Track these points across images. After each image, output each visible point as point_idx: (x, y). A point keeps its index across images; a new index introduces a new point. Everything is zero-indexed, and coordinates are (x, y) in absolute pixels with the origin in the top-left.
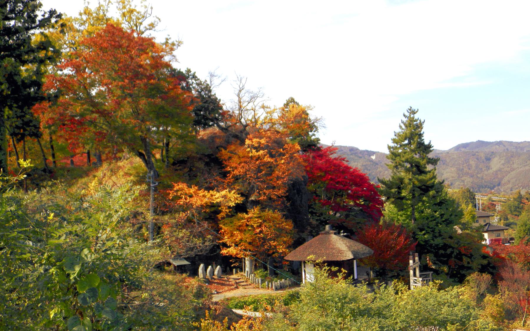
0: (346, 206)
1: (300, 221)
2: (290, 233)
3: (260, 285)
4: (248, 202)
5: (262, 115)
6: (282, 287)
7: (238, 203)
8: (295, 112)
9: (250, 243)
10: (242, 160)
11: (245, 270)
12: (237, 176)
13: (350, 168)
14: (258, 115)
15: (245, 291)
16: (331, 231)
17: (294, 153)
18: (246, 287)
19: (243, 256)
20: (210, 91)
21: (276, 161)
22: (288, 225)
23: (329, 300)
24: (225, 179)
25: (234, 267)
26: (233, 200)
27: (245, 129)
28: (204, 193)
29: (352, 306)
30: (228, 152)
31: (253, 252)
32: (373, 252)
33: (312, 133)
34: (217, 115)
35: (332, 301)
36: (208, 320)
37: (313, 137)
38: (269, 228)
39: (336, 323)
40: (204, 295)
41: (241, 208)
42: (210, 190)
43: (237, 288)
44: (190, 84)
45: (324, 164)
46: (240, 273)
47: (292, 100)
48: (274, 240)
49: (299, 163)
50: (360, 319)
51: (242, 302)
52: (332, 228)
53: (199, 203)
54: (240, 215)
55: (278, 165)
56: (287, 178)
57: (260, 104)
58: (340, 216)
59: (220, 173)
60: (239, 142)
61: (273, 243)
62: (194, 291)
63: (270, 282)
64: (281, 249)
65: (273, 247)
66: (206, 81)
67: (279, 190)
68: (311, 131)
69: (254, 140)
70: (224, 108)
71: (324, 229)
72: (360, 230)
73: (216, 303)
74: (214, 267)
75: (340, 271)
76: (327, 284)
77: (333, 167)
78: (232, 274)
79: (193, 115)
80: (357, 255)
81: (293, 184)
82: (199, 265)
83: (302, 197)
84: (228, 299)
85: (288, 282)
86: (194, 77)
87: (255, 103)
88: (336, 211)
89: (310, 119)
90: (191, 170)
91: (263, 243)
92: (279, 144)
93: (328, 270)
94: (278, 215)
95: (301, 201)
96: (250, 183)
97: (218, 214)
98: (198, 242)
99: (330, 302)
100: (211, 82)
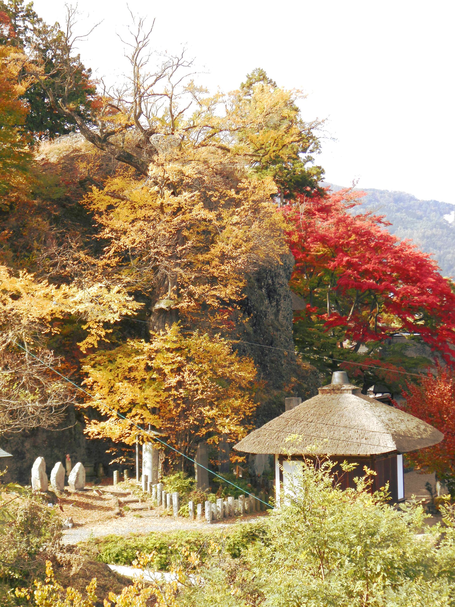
0: (383, 329)
1: (272, 362)
2: (248, 389)
3: (175, 509)
4: (151, 313)
5: (188, 109)
6: (228, 516)
7: (127, 315)
8: (267, 102)
9: (153, 411)
10: (140, 213)
11: (140, 474)
12: (127, 251)
13: (395, 240)
14: (180, 109)
15: (140, 522)
16: (346, 387)
17: (262, 201)
18: (143, 513)
19: (136, 441)
20: (67, 49)
21: (219, 218)
22: (246, 372)
23: (334, 539)
24: (98, 258)
25: (116, 466)
26: (115, 308)
27: (148, 141)
28: (47, 290)
29: (387, 552)
30: (107, 194)
31: (159, 430)
32: (442, 437)
33: (307, 154)
34: (82, 108)
35: (342, 542)
36: (50, 583)
37: (308, 165)
38: (199, 376)
39: (350, 594)
40: (43, 530)
41: (132, 328)
42: (63, 282)
43: (120, 514)
44: (20, 32)
45: (333, 229)
46: (128, 482)
47: (262, 77)
48: (211, 404)
49: (273, 224)
50: (407, 585)
51: (133, 549)
52: (349, 379)
53: (36, 313)
54: (133, 344)
55: (224, 228)
56: (243, 257)
57: (186, 82)
58: (369, 353)
59: (86, 244)
60: (132, 170)
61: (209, 412)
62: (19, 519)
63: (198, 502)
64: (228, 426)
65: (207, 421)
66: (57, 24)
67: (225, 286)
68: (304, 151)
69: (169, 167)
70: (99, 90)
71: (329, 382)
72: (412, 385)
73: (71, 549)
74: (68, 466)
75: (359, 472)
76: (330, 502)
77: (353, 237)
78: (112, 484)
79: (25, 103)
80: (405, 445)
81: (258, 273)
82: (33, 461)
83: (277, 305)
84: (97, 542)
85: (240, 504)
86: (30, 14)
87: (174, 80)
88: (360, 342)
89: (301, 122)
90: (18, 234)
91: (184, 410)
92: (229, 177)
93: (334, 469)
94: (221, 346)
95: (276, 314)
96: (155, 269)
97: (81, 340)
98: (30, 401)
99: (337, 544)
100: (69, 27)
